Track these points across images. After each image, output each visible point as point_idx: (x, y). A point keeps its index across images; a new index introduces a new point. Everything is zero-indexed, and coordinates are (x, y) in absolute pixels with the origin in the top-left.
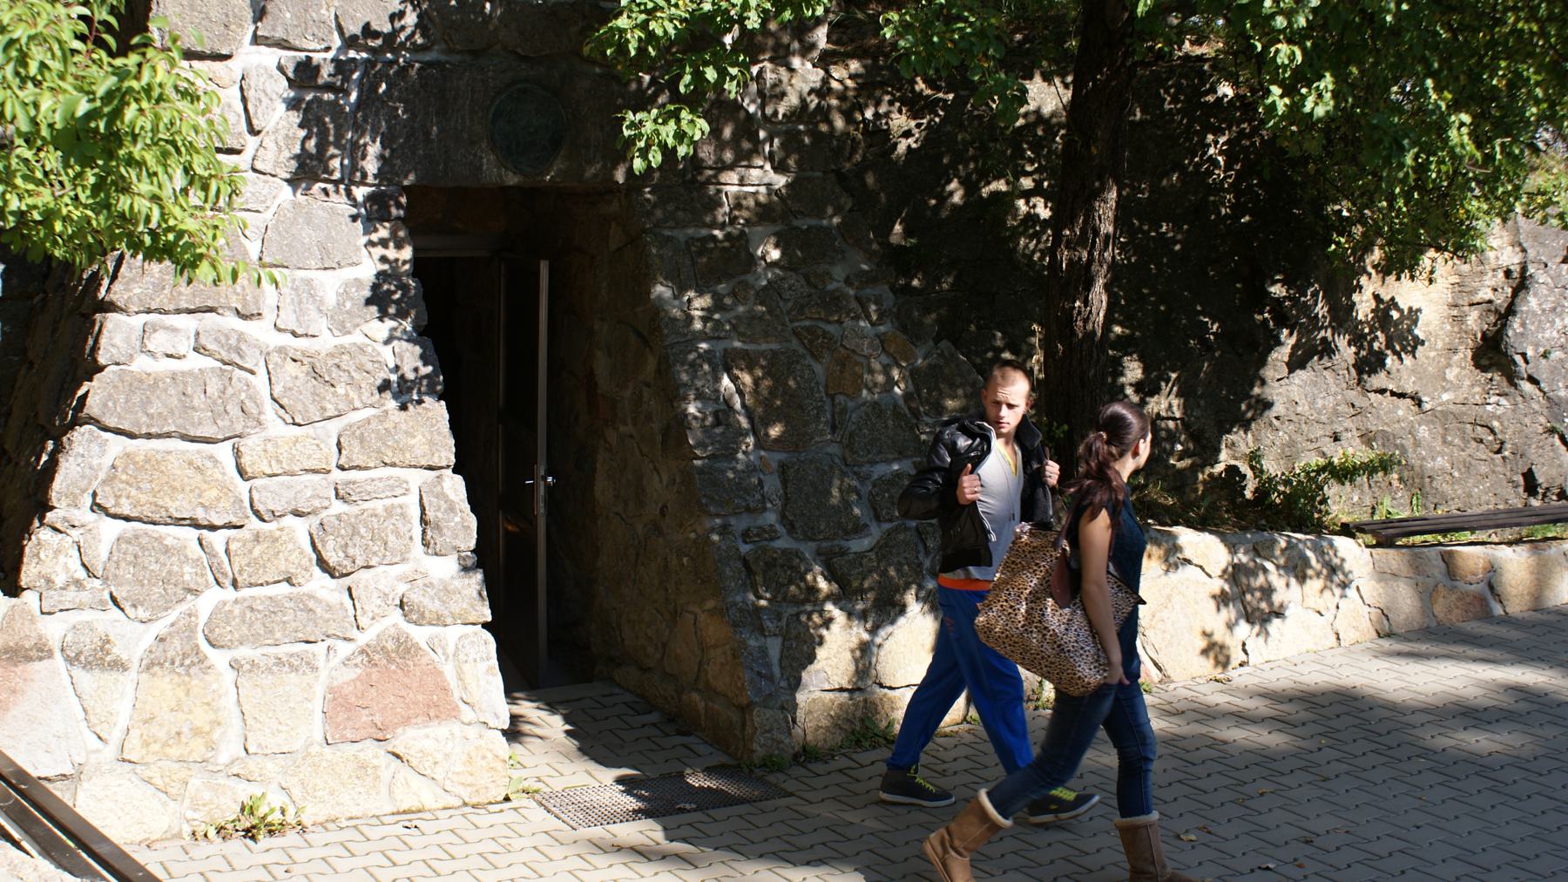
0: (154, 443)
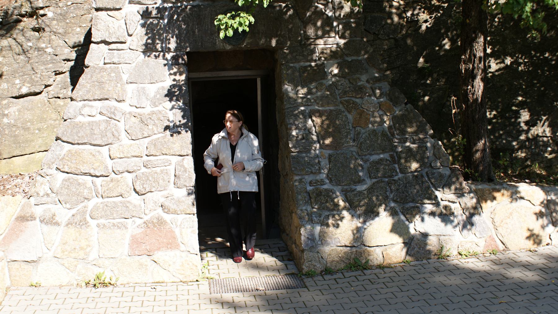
0: (81, 147)
